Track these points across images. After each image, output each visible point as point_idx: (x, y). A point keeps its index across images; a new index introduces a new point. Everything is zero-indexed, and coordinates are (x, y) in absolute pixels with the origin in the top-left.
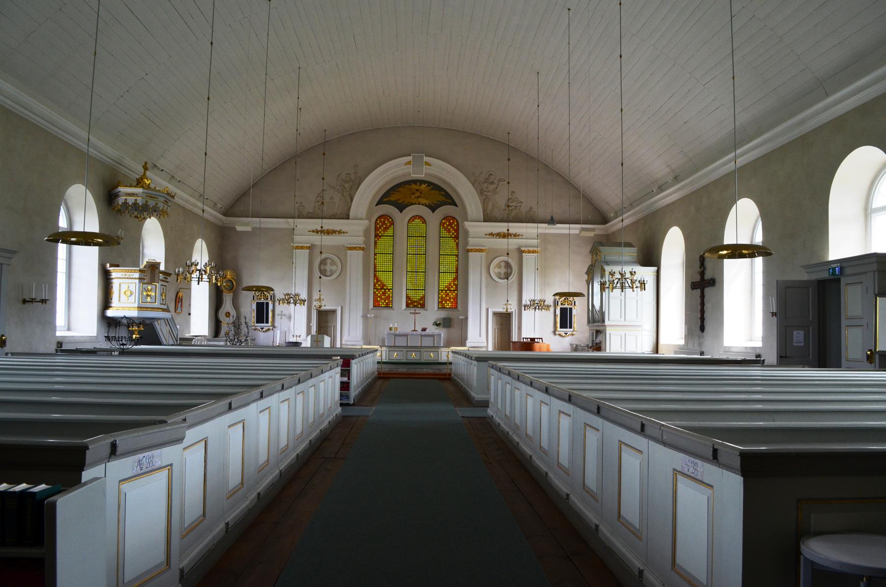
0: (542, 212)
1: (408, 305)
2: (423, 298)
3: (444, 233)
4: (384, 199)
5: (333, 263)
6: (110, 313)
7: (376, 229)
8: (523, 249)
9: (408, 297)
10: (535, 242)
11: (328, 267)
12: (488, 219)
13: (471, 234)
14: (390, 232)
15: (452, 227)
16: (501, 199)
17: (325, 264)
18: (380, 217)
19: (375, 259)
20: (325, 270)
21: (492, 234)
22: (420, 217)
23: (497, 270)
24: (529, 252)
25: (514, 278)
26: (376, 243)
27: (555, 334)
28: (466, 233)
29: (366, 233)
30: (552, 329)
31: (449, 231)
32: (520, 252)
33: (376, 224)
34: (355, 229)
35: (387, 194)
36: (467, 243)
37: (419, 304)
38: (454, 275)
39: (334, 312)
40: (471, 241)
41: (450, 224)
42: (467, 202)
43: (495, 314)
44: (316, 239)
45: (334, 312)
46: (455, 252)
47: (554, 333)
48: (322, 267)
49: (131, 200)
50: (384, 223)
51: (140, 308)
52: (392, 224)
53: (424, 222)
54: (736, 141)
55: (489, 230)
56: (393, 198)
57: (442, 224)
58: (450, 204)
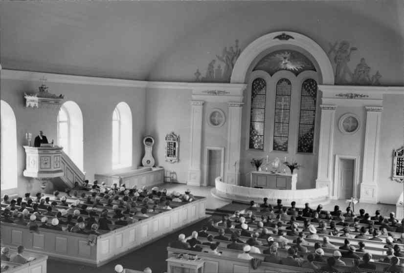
0: (384, 78)
1: (274, 149)
2: (287, 143)
3: (305, 93)
4: (256, 66)
5: (220, 115)
6: (26, 174)
7: (253, 89)
8: (367, 108)
9: (274, 142)
10: (380, 102)
11: (216, 118)
12: (338, 82)
13: (323, 95)
14: (263, 92)
15: (311, 88)
16: (352, 65)
17: (215, 116)
18: (256, 80)
19: (251, 112)
20: (214, 120)
21: (341, 95)
22: (287, 80)
23: (346, 124)
24: (373, 110)
25: (359, 130)
26: (252, 100)
27: (392, 180)
28: (321, 93)
29: (245, 92)
30: (389, 175)
31: (309, 91)
32: (365, 111)
33: (253, 85)
34: (236, 90)
35: (262, 61)
36: (321, 103)
37: (284, 148)
38: (310, 127)
39: (220, 151)
40: (324, 100)
41: (311, 85)
42: (321, 67)
43: (341, 159)
44: (210, 99)
45: (220, 151)
46: (313, 108)
47: (391, 178)
48: (213, 118)
49: (32, 104)
50: (259, 84)
51: (40, 172)
52: (265, 85)
53: (289, 83)
54: (32, 252)
55: (339, 92)
56: (266, 64)
57: (304, 85)
58: (312, 70)
